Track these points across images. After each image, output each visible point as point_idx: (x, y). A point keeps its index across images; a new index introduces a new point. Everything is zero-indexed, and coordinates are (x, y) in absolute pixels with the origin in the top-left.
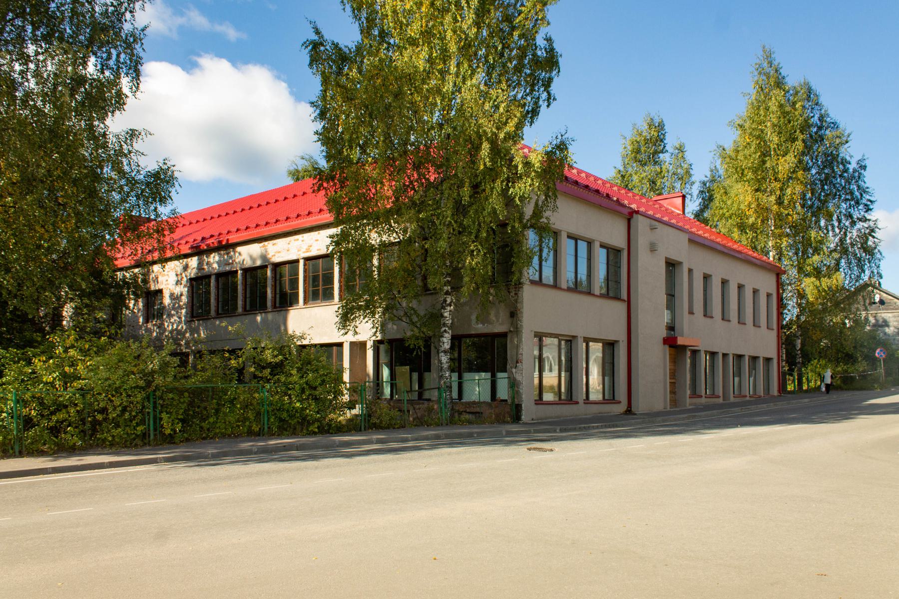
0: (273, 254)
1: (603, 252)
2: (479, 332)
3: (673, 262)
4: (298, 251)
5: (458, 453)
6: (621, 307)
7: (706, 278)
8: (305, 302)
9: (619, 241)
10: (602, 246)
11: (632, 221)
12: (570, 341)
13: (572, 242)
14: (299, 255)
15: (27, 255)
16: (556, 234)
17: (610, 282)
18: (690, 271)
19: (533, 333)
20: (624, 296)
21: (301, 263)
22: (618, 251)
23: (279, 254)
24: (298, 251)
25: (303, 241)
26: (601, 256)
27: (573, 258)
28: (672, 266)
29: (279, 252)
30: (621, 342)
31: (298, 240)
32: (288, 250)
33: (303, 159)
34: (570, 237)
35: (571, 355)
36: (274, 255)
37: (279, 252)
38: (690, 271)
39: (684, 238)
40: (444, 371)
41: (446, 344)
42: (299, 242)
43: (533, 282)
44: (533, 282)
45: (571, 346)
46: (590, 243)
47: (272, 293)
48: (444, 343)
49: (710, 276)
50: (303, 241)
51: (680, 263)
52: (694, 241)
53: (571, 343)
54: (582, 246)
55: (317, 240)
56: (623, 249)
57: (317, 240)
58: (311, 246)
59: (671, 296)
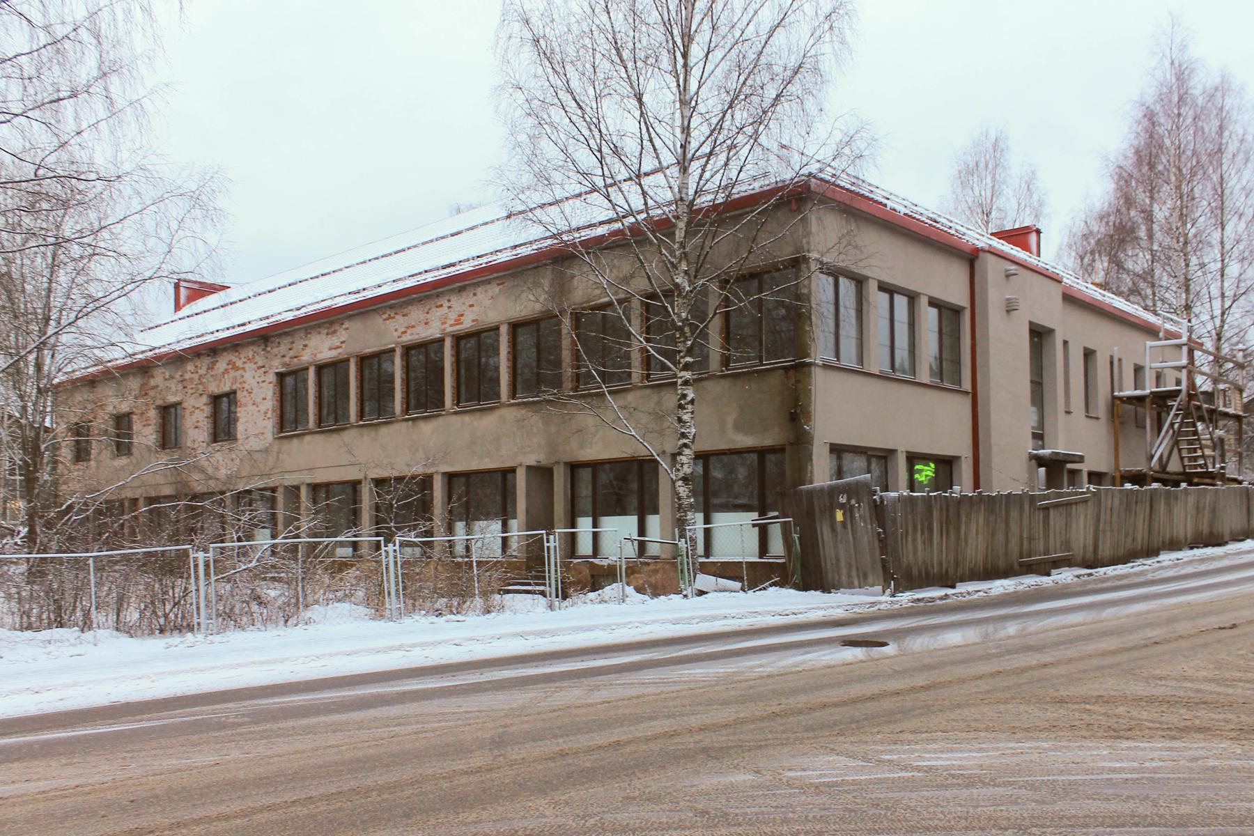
0: (403, 330)
1: (933, 313)
2: (738, 446)
3: (1039, 330)
4: (443, 323)
5: (726, 704)
6: (965, 404)
7: (1089, 354)
8: (458, 400)
9: (957, 295)
10: (933, 303)
11: (977, 265)
12: (885, 458)
13: (885, 297)
14: (444, 330)
15: (49, 624)
16: (860, 282)
17: (944, 363)
18: (1065, 343)
19: (828, 446)
20: (967, 385)
21: (448, 343)
22: (956, 311)
23: (414, 330)
24: (443, 323)
25: (449, 307)
26: (929, 318)
27: (887, 323)
28: (1039, 335)
29: (413, 327)
30: (963, 459)
31: (441, 306)
32: (426, 324)
33: (459, 211)
34: (883, 287)
35: (887, 481)
36: (405, 332)
37: (413, 327)
38: (1065, 343)
39: (1056, 292)
40: (685, 512)
41: (685, 467)
42: (444, 310)
43: (827, 366)
44: (827, 366)
45: (886, 467)
46: (912, 298)
47: (402, 405)
48: (682, 464)
49: (1094, 352)
50: (449, 307)
51: (1050, 332)
52: (1071, 299)
53: (886, 462)
54: (901, 302)
55: (471, 306)
56: (963, 308)
57: (471, 306)
58: (462, 315)
59: (1038, 385)
